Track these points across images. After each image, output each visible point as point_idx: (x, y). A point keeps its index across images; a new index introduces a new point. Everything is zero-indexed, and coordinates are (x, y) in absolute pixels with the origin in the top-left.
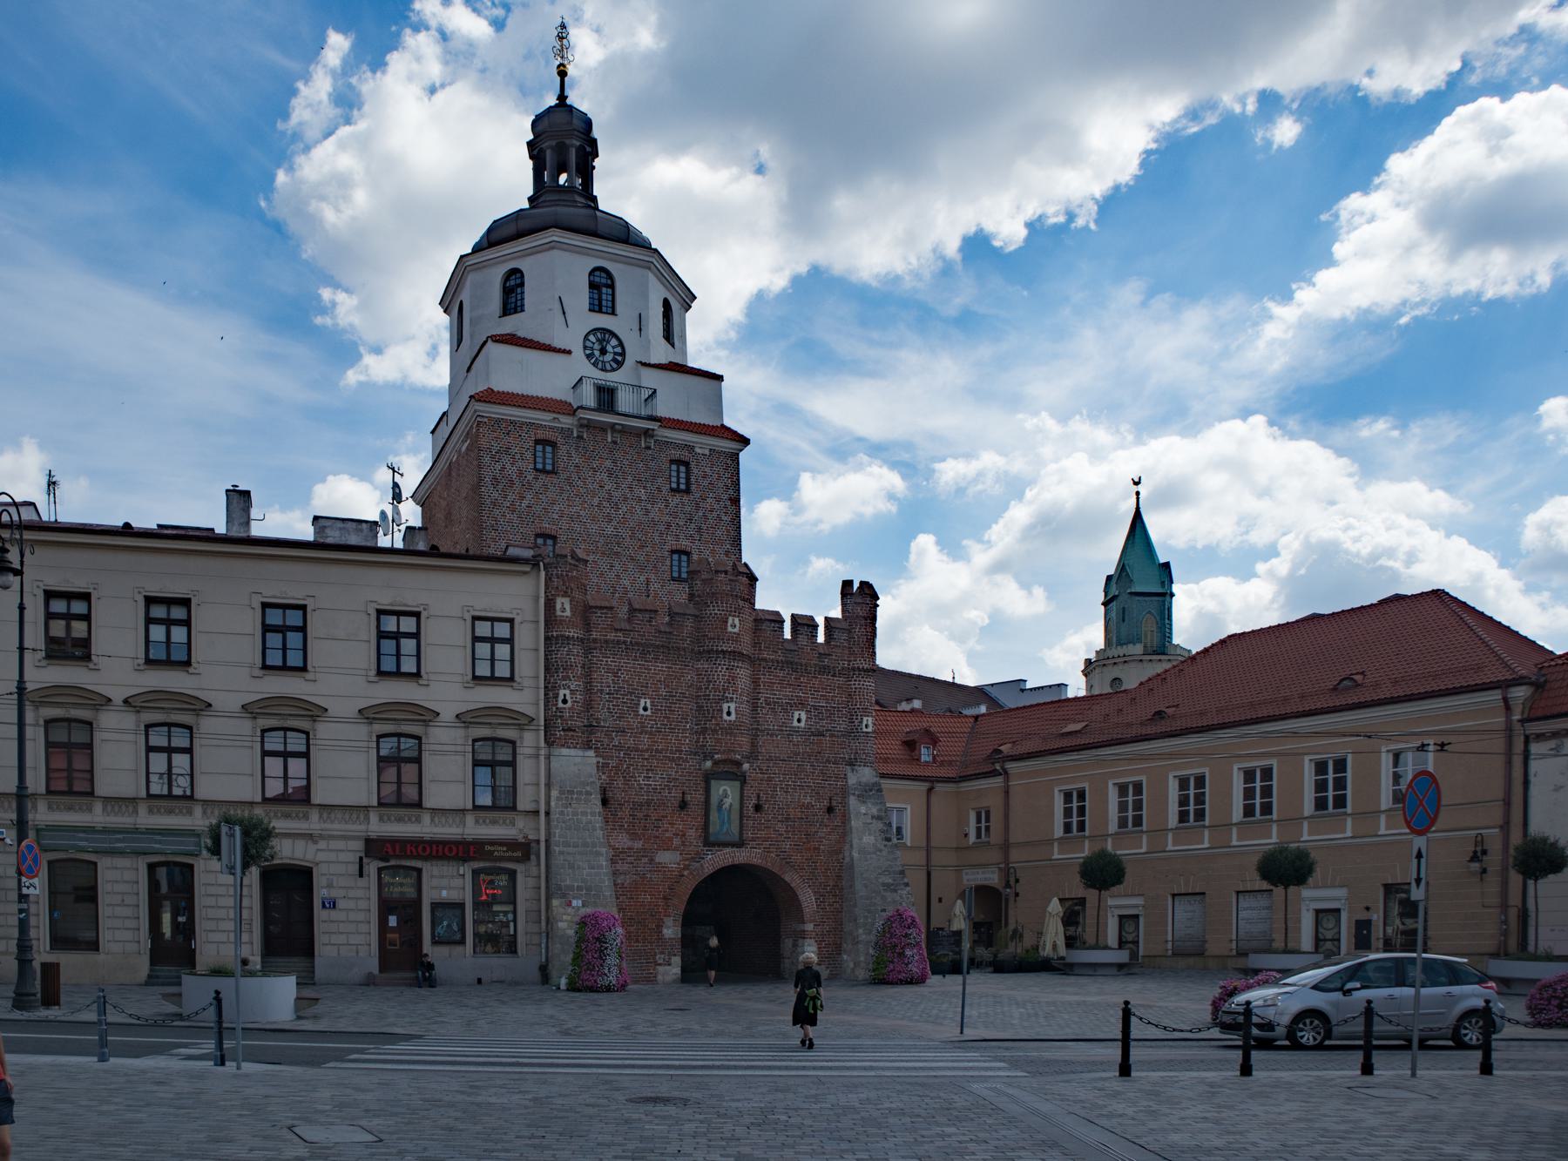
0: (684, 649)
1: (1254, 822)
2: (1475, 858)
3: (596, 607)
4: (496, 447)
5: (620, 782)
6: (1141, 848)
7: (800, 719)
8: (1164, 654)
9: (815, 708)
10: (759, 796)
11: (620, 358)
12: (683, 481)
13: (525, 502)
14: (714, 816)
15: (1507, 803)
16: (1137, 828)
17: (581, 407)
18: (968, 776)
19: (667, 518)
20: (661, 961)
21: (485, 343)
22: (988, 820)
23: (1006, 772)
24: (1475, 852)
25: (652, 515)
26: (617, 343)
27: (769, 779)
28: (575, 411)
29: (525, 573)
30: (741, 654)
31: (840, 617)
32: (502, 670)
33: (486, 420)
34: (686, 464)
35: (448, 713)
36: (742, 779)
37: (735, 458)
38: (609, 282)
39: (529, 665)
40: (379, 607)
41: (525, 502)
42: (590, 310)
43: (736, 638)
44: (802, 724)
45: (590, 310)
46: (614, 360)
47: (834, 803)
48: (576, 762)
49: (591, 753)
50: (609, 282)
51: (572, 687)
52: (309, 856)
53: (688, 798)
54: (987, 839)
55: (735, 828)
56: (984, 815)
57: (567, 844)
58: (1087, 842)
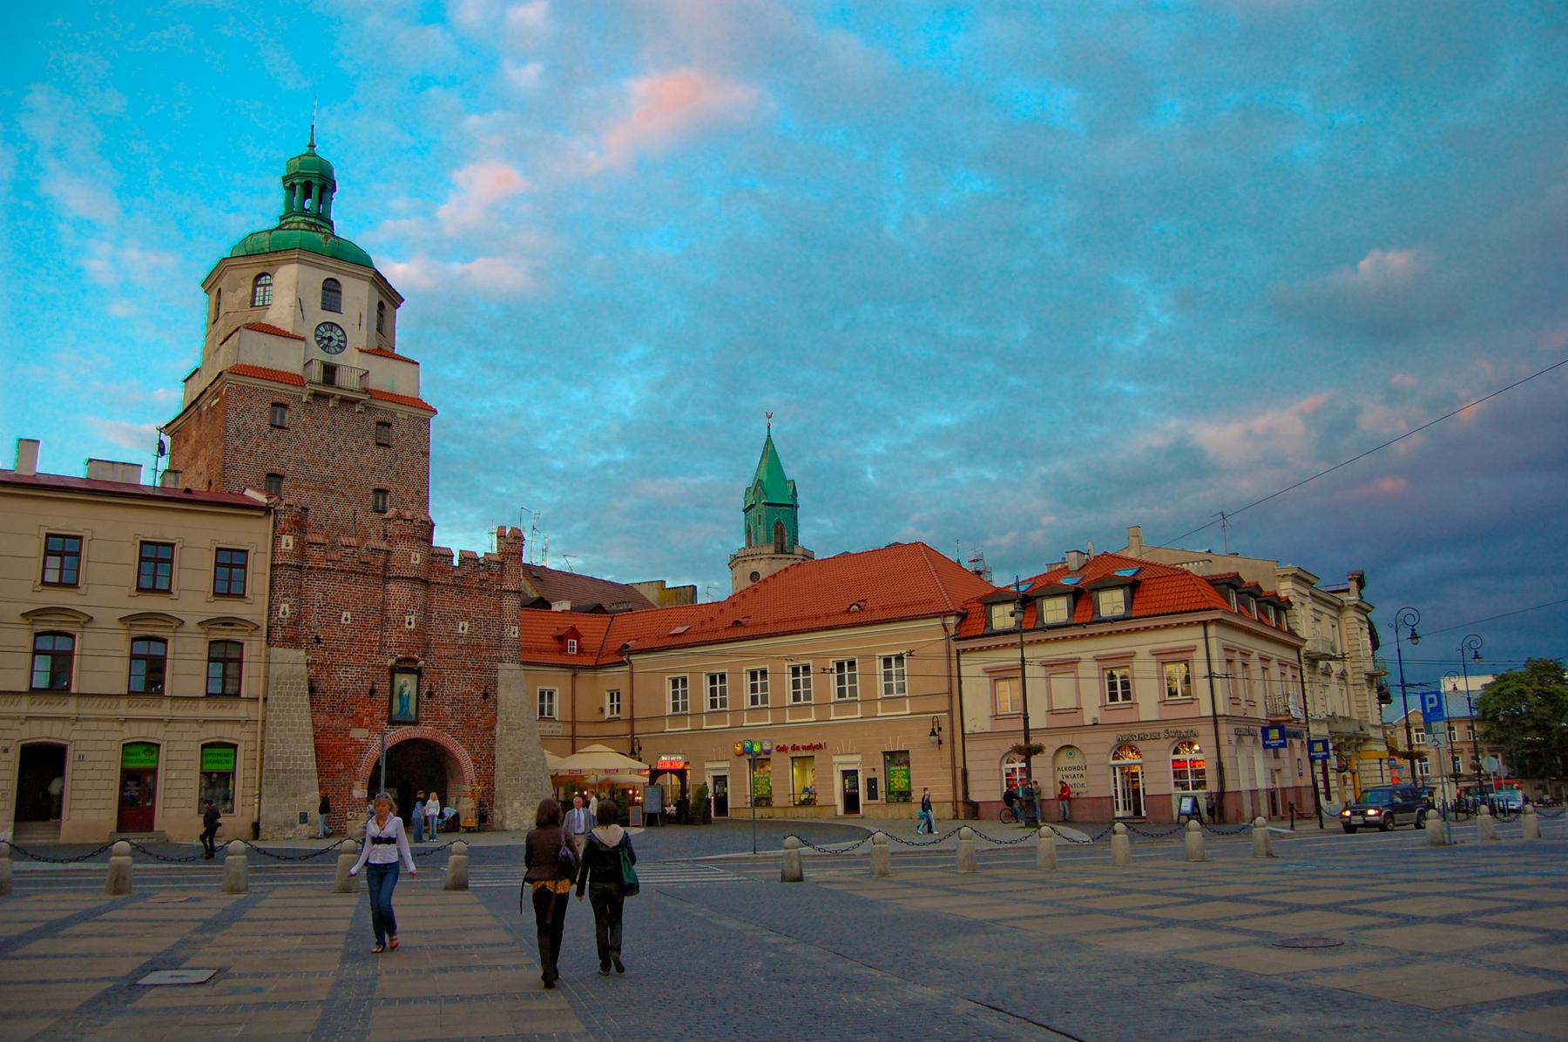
0: (377, 575)
1: (757, 709)
2: (933, 733)
4: (241, 406)
6: (905, 710)
7: (463, 627)
8: (793, 554)
11: (342, 344)
13: (261, 450)
14: (396, 702)
15: (950, 694)
16: (883, 689)
18: (24, 872)
19: (373, 465)
20: (350, 817)
22: (618, 700)
23: (630, 662)
24: (933, 729)
25: (360, 462)
26: (341, 333)
27: (439, 673)
29: (259, 517)
33: (234, 386)
35: (191, 622)
36: (419, 673)
37: (427, 422)
40: (143, 539)
41: (261, 450)
42: (322, 309)
44: (465, 631)
46: (338, 345)
48: (292, 661)
49: (302, 653)
51: (291, 603)
52: (65, 736)
53: (377, 687)
54: (618, 715)
56: (615, 695)
57: (280, 724)
58: (689, 718)
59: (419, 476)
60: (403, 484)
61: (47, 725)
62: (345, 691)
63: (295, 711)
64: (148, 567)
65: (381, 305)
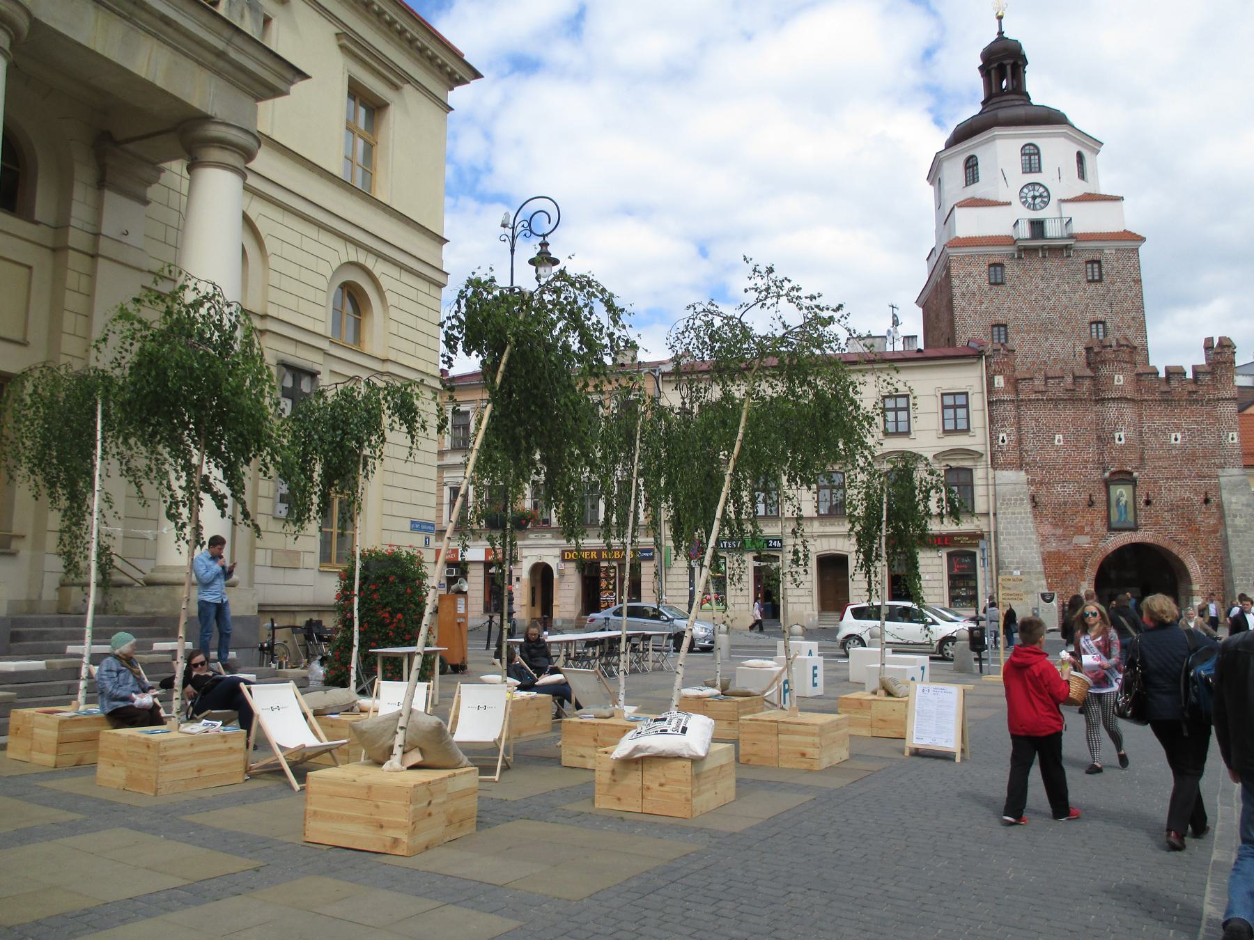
0: (1085, 400)
3: (1021, 379)
5: (1044, 491)
7: (1176, 438)
9: (1188, 430)
10: (1148, 494)
11: (1046, 200)
12: (1096, 274)
14: (1114, 511)
17: (1019, 239)
19: (1087, 301)
21: (953, 209)
25: (1073, 301)
28: (1015, 241)
29: (973, 363)
30: (1126, 399)
31: (1204, 363)
32: (962, 425)
34: (1099, 262)
36: (1133, 482)
38: (1036, 151)
39: (978, 417)
42: (1023, 173)
43: (1121, 389)
45: (1023, 173)
47: (1209, 496)
48: (1013, 479)
49: (1023, 473)
50: (1036, 151)
55: (1130, 517)
57: (1009, 534)
59: (1133, 303)
60: (1117, 313)
61: (833, 541)
62: (1065, 503)
63: (1022, 523)
64: (950, 413)
65: (1080, 157)
